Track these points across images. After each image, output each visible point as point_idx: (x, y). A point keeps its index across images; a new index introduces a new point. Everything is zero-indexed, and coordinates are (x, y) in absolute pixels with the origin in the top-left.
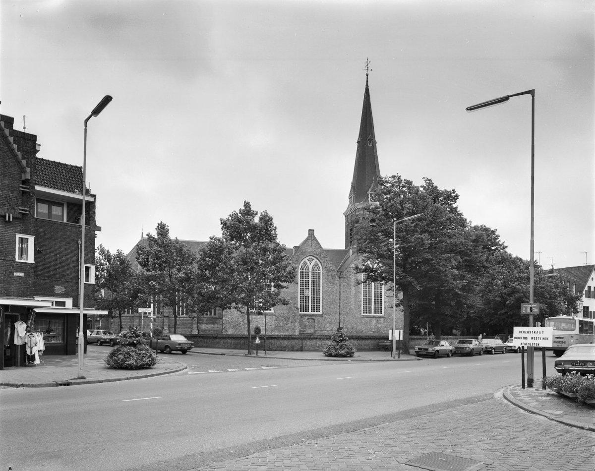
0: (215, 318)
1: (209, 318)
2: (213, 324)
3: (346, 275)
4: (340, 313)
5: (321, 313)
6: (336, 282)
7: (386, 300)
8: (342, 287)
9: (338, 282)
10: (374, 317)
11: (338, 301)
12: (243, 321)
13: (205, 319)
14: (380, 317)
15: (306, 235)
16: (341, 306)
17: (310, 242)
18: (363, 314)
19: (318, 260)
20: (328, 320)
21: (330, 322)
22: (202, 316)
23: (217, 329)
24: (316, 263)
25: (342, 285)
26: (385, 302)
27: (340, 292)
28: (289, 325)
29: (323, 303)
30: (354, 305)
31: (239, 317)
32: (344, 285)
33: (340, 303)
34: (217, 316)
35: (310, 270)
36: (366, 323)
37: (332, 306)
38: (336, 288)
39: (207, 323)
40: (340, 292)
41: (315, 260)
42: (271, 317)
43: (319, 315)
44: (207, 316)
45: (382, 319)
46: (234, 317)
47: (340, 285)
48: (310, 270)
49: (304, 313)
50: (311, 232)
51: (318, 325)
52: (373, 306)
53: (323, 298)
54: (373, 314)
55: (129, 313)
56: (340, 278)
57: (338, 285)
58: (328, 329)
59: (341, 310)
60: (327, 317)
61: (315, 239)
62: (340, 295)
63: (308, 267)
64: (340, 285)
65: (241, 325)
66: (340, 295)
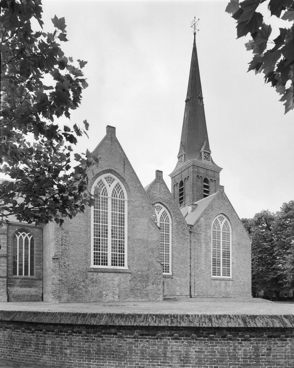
0: (32, 279)
1: (25, 279)
2: (30, 286)
3: (196, 229)
4: (190, 275)
5: (170, 274)
6: (187, 237)
7: (234, 261)
8: (192, 244)
9: (189, 237)
10: (223, 280)
11: (189, 260)
12: (84, 281)
13: (18, 281)
14: (229, 280)
15: (104, 133)
16: (192, 266)
17: (158, 186)
18: (93, 266)
19: (167, 208)
20: (179, 282)
21: (180, 286)
22: (14, 276)
23: (35, 294)
24: (118, 186)
25: (192, 242)
26: (233, 263)
27: (190, 249)
28: (149, 288)
29: (172, 262)
30: (204, 266)
31: (78, 275)
32: (194, 242)
33: (190, 262)
34: (34, 277)
35: (110, 195)
36: (216, 286)
37: (182, 266)
38: (187, 245)
39: (21, 286)
40: (190, 249)
41: (164, 209)
42: (125, 275)
43: (169, 277)
44: (21, 277)
45: (231, 282)
46: (69, 274)
47: (190, 241)
48: (110, 195)
49: (101, 267)
50: (111, 130)
51: (168, 288)
52: (221, 267)
53: (172, 256)
54: (222, 277)
55: (22, 274)
56: (190, 232)
57: (189, 241)
58: (178, 294)
59: (192, 271)
60: (178, 278)
61: (117, 141)
62: (191, 253)
63: (105, 191)
64: (190, 241)
65: (81, 287)
66: (191, 253)
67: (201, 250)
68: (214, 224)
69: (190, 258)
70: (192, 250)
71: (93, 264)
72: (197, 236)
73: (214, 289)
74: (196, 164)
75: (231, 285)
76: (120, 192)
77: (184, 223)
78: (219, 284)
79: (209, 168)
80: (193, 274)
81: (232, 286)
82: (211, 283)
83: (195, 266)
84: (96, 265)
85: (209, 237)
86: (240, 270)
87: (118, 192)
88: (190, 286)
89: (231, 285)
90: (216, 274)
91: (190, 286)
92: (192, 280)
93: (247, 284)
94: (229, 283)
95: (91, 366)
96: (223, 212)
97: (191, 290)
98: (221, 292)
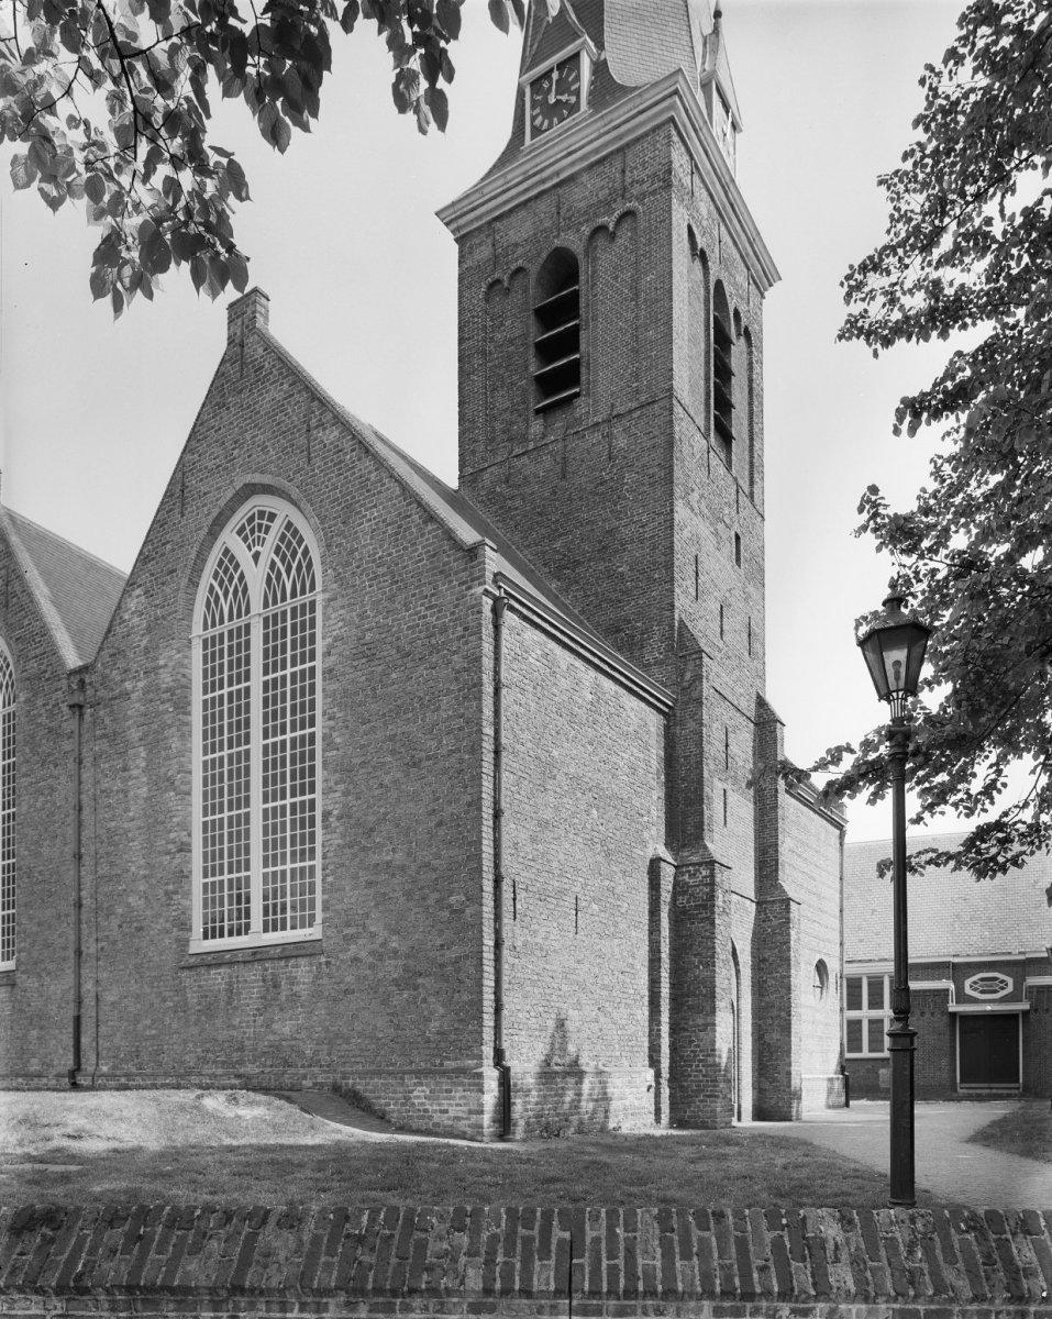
10: (257, 955)
18: (199, 945)
36: (209, 1011)
45: (303, 971)
67: (125, 792)
68: (212, 588)
69: (79, 857)
70: (86, 812)
71: (201, 936)
72: (107, 721)
73: (194, 1030)
74: (478, 212)
75: (302, 989)
76: (294, 566)
77: (56, 677)
78: (223, 997)
79: (573, 164)
80: (90, 948)
81: (317, 994)
82: (180, 990)
83: (100, 898)
84: (273, 931)
85: (166, 696)
86: (374, 858)
87: (226, 594)
88: (78, 1020)
89: (302, 989)
90: (284, 921)
91: (78, 1020)
92: (88, 986)
93: (442, 966)
94: (292, 981)
95: (918, 1311)
96: (249, 478)
97: (83, 1040)
98: (241, 1049)
